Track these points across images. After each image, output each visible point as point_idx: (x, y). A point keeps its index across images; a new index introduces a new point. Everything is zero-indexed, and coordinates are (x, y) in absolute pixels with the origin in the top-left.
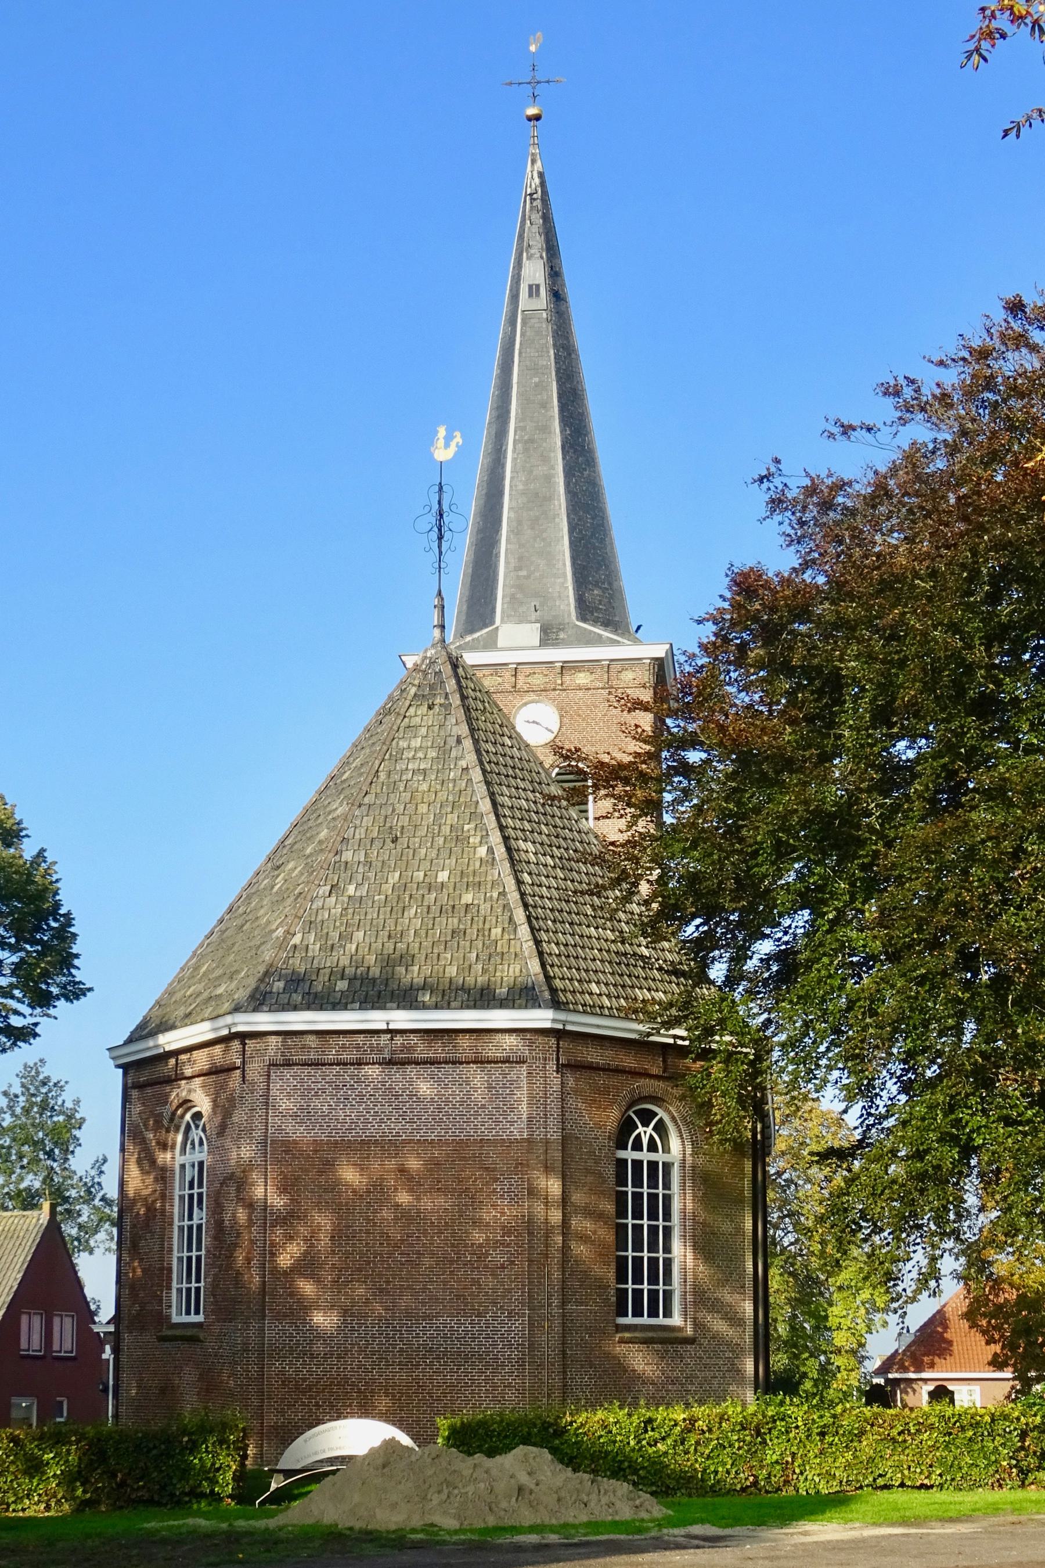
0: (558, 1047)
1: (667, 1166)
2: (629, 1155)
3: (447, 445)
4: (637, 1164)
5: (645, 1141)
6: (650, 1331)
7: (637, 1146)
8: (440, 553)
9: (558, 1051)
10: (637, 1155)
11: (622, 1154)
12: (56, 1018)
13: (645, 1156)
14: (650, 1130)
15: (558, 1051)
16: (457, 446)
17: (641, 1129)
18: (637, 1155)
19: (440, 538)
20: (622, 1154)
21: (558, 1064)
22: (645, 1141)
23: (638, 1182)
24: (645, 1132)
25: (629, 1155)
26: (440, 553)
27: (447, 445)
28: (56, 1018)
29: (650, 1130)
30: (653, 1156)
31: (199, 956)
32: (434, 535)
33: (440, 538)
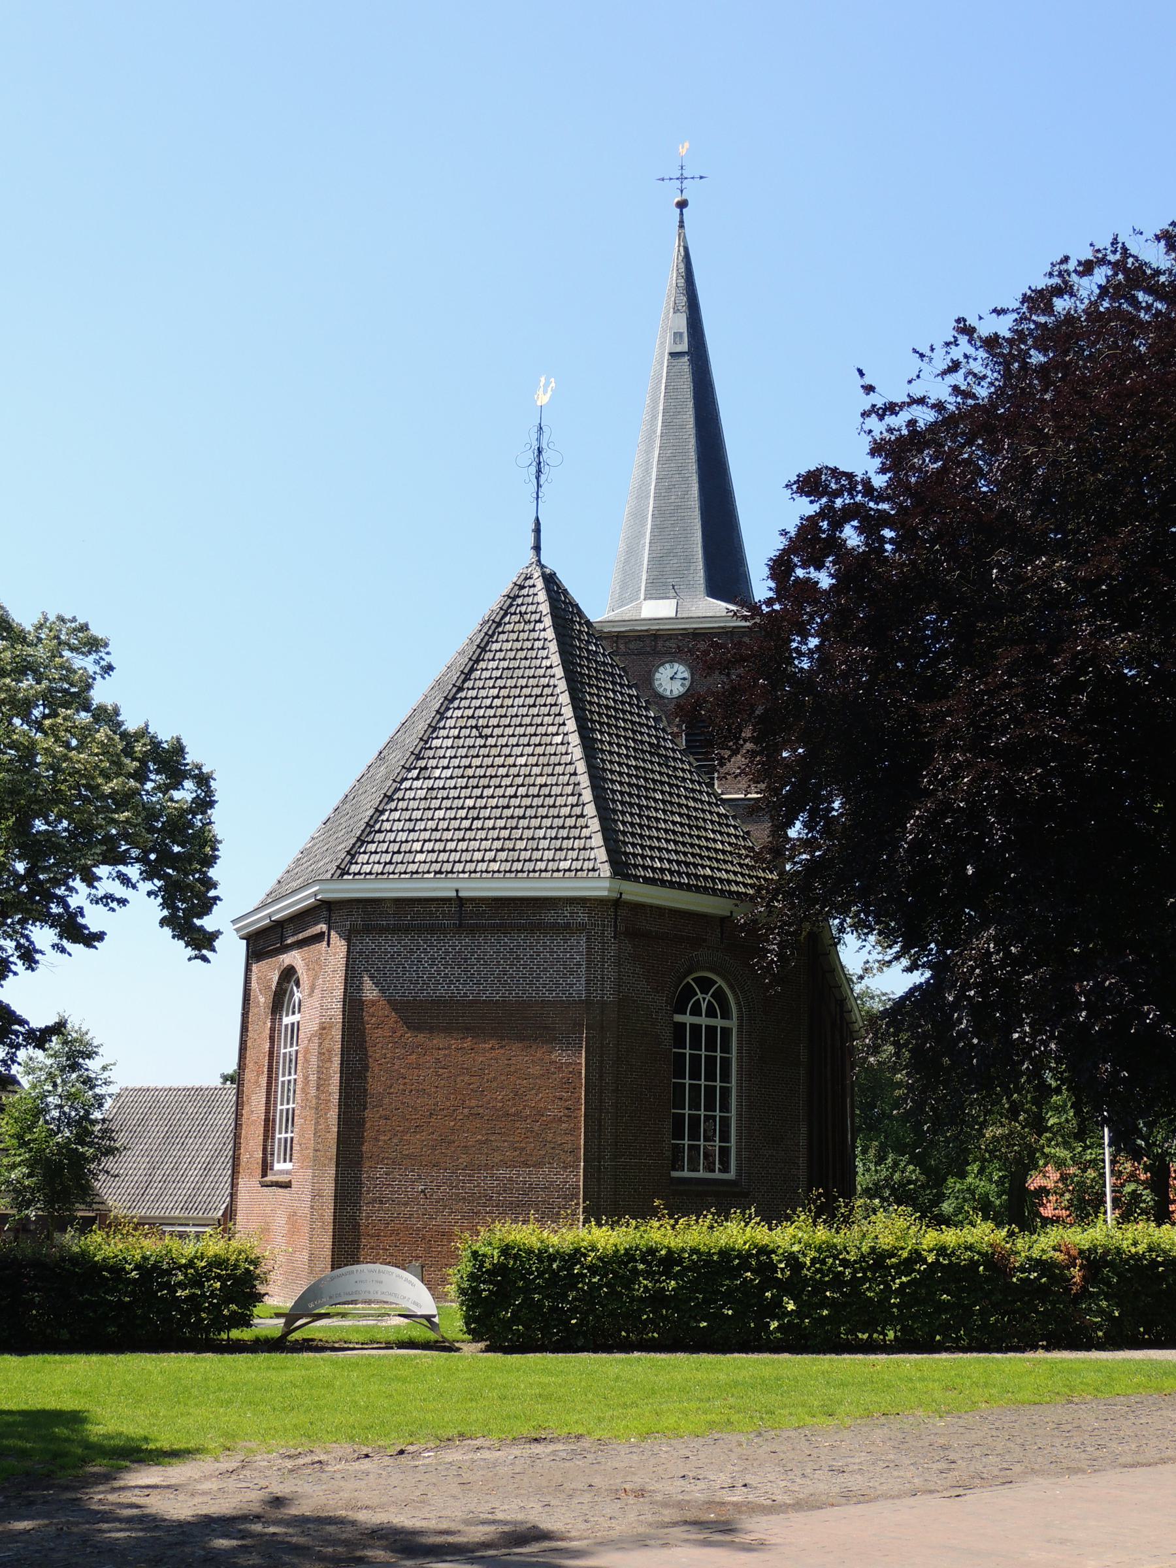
0: (616, 915)
1: (726, 1032)
2: (687, 1019)
3: (545, 392)
4: (696, 1028)
5: (704, 1006)
6: (796, 1277)
7: (696, 1011)
8: (539, 486)
9: (616, 919)
10: (696, 1020)
11: (678, 1018)
12: (70, 955)
13: (703, 1021)
14: (708, 997)
15: (616, 919)
16: (912, 423)
17: (700, 996)
18: (696, 1020)
19: (539, 471)
20: (678, 1018)
21: (615, 931)
22: (704, 1006)
23: (696, 1045)
24: (704, 999)
25: (687, 1019)
26: (539, 486)
27: (545, 392)
28: (70, 955)
29: (708, 997)
30: (712, 1022)
31: (626, 1347)
32: (533, 469)
33: (539, 471)
